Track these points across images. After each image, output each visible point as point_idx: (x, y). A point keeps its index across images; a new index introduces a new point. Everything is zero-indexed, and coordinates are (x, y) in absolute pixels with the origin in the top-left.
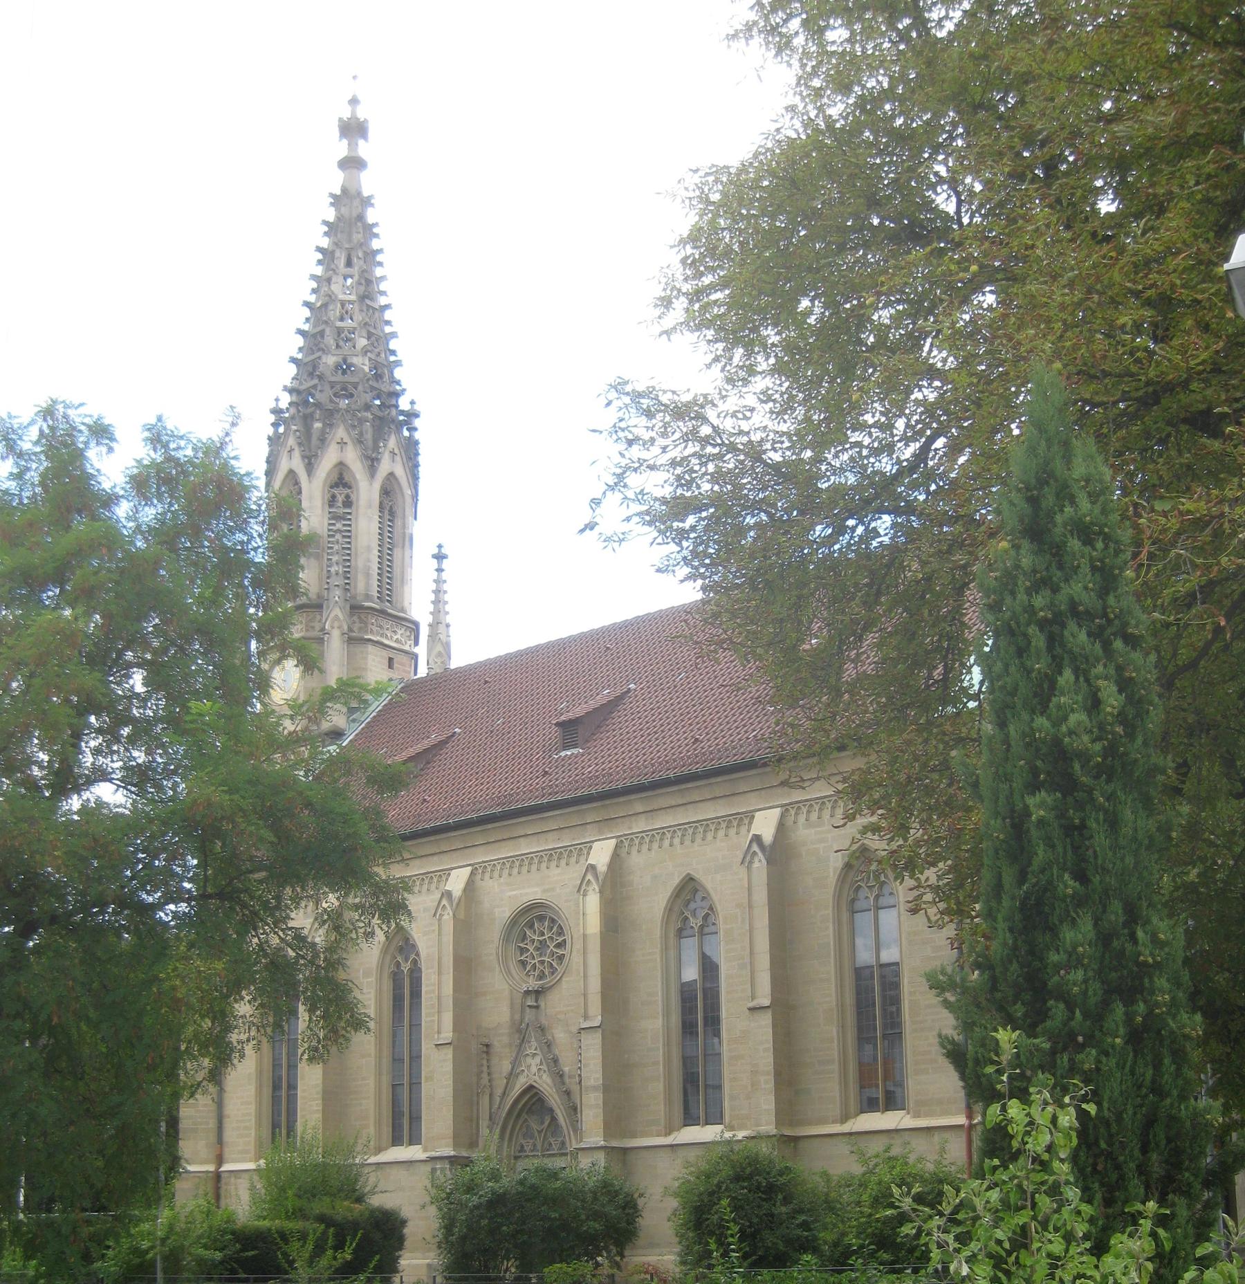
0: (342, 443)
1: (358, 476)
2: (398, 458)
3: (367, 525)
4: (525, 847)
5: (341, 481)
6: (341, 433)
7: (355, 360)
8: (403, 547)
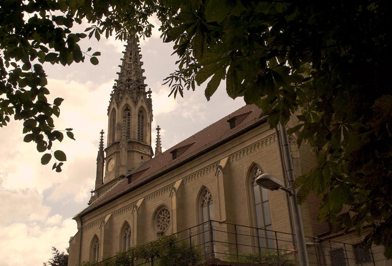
0: (127, 99)
1: (131, 107)
2: (144, 102)
3: (134, 120)
4: (158, 188)
5: (127, 109)
6: (127, 96)
7: (132, 78)
8: (146, 126)
